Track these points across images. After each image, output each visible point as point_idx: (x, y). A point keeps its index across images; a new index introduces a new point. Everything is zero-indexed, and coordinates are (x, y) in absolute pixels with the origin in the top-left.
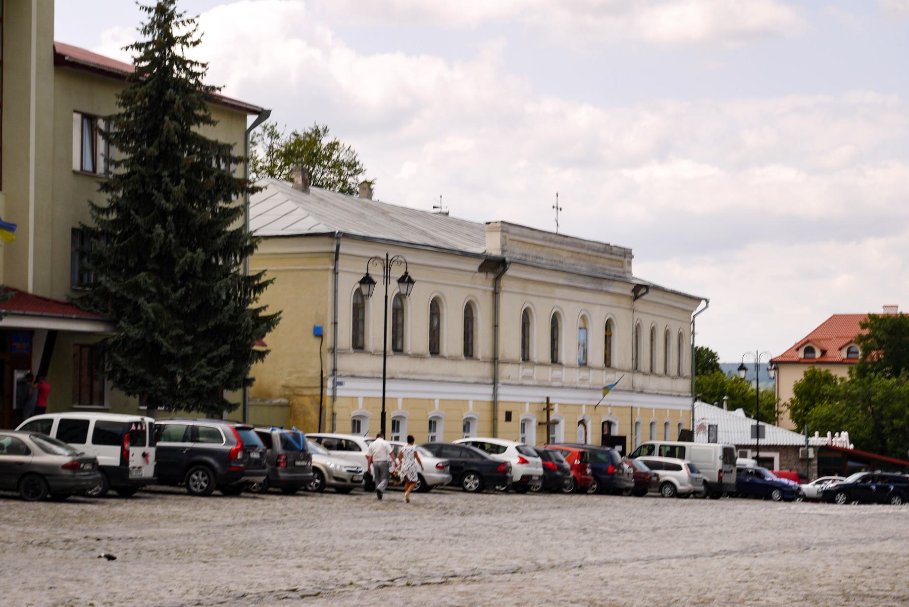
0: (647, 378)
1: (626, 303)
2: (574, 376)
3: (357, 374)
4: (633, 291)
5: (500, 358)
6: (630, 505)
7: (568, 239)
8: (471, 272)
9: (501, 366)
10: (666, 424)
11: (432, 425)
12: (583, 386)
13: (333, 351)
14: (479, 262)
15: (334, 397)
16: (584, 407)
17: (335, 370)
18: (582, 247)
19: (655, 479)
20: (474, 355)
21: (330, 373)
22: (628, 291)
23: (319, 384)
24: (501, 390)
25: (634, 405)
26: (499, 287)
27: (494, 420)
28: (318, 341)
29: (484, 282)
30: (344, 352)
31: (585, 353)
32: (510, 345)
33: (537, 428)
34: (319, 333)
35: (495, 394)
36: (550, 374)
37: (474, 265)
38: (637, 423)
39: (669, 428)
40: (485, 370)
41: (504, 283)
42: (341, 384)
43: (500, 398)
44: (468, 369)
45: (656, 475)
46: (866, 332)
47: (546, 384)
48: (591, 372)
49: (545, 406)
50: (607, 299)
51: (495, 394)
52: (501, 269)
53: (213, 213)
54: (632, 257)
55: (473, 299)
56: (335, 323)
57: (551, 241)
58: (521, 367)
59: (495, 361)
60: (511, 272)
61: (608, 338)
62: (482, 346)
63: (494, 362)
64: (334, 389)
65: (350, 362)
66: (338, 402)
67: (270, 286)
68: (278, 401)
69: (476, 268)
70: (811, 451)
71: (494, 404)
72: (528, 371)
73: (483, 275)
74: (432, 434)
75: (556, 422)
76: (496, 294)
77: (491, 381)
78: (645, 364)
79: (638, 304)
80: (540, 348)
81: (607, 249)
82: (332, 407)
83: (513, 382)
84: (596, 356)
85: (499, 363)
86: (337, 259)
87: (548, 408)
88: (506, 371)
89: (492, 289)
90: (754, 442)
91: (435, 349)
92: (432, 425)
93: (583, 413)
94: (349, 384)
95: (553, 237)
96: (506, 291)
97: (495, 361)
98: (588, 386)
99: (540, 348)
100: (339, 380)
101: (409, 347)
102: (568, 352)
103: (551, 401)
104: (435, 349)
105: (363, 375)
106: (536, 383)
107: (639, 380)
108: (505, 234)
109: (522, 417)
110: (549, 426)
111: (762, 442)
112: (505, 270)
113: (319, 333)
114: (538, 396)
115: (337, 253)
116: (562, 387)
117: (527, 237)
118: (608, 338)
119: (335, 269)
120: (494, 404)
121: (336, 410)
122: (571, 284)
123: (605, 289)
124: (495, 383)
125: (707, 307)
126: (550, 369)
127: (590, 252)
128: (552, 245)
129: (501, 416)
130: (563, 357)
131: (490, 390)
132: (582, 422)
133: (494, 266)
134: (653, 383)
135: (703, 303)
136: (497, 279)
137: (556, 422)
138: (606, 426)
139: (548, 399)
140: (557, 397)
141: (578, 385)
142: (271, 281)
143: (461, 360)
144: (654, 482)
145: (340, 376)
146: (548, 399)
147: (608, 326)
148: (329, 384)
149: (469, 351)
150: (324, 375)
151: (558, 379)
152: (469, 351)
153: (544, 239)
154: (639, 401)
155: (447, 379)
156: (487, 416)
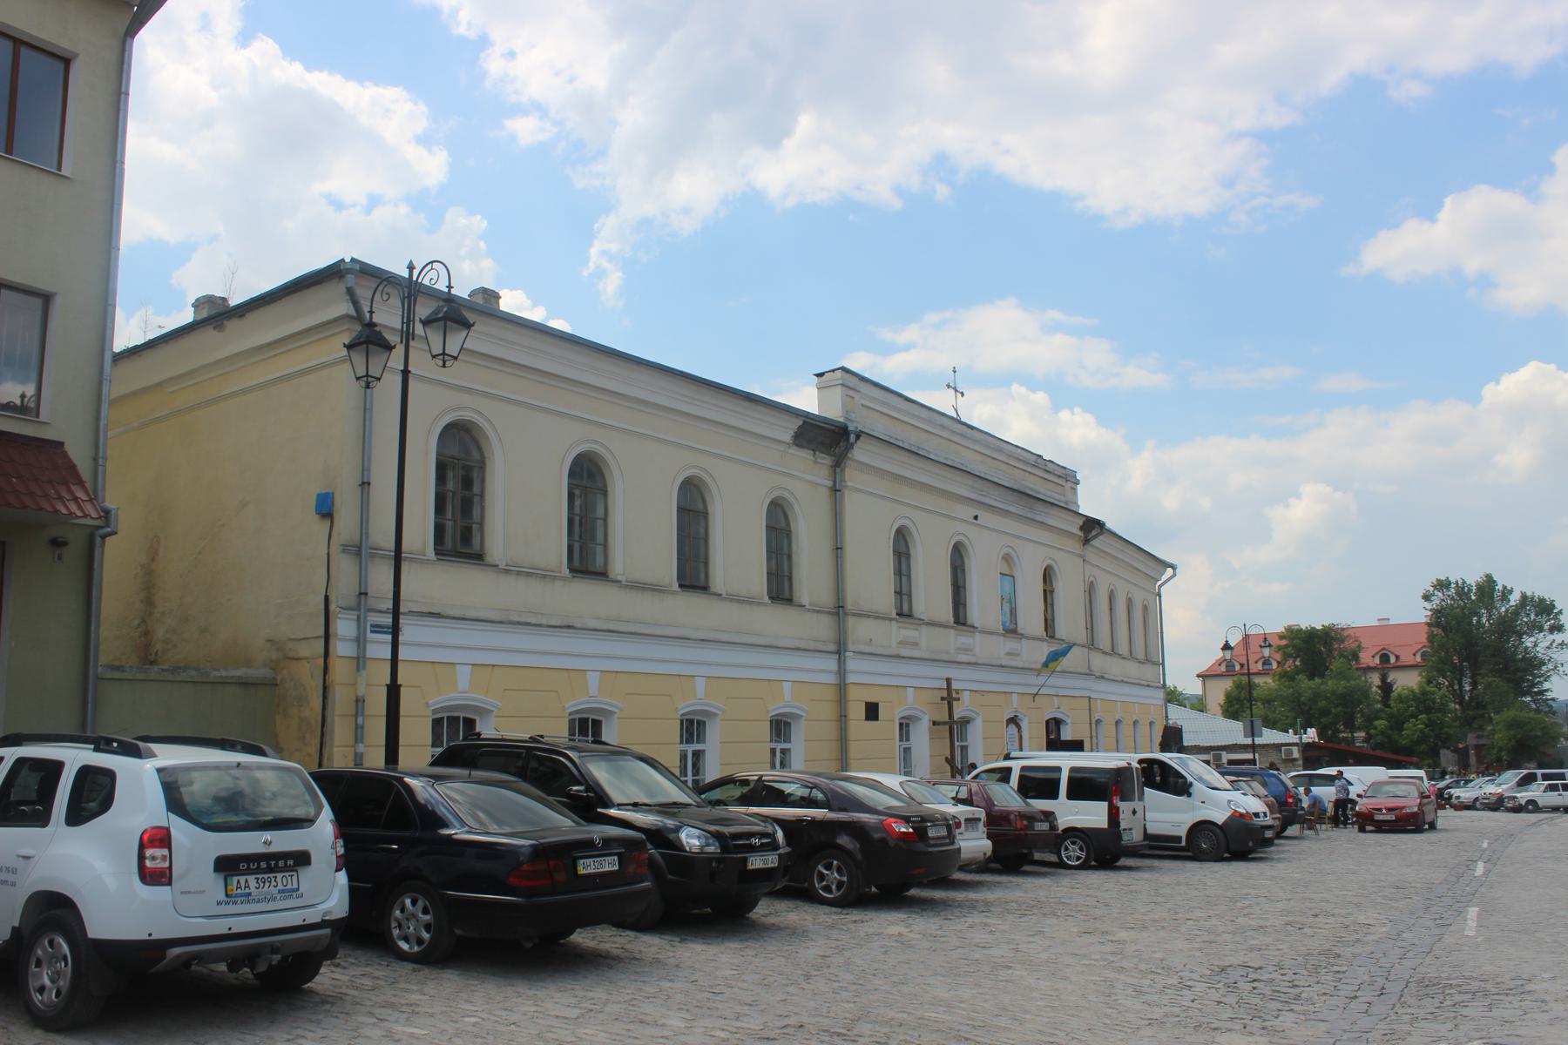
0: (1108, 658)
1: (1074, 546)
2: (999, 648)
4: (1082, 528)
5: (849, 606)
6: (865, 929)
7: (974, 433)
9: (851, 621)
10: (1135, 723)
11: (693, 728)
12: (1013, 663)
16: (787, 687)
18: (1000, 451)
19: (1042, 827)
22: (1074, 527)
23: (322, 632)
24: (852, 664)
26: (843, 480)
27: (842, 718)
31: (1013, 613)
32: (871, 581)
33: (931, 732)
34: (326, 509)
35: (841, 672)
36: (952, 640)
37: (786, 430)
38: (1098, 721)
39: (1122, 727)
40: (822, 627)
41: (852, 476)
43: (851, 678)
45: (1049, 816)
46: (1284, 642)
47: (946, 657)
48: (1024, 642)
49: (945, 694)
50: (1044, 536)
51: (841, 672)
54: (1077, 483)
55: (786, 495)
57: (942, 427)
60: (861, 453)
61: (1048, 594)
62: (811, 578)
69: (787, 436)
70: (1295, 749)
71: (842, 688)
72: (908, 632)
74: (905, 744)
75: (965, 722)
76: (835, 490)
77: (832, 647)
78: (1103, 641)
79: (1090, 553)
80: (932, 595)
81: (1038, 463)
83: (879, 651)
84: (1031, 619)
85: (846, 614)
87: (950, 698)
88: (860, 631)
89: (830, 483)
90: (1249, 741)
91: (693, 574)
92: (693, 728)
93: (1015, 705)
95: (947, 422)
96: (450, 287)
97: (839, 610)
98: (1020, 665)
99: (932, 595)
101: (621, 561)
102: (983, 605)
103: (955, 686)
104: (693, 574)
106: (926, 655)
107: (1098, 662)
108: (851, 393)
109: (898, 715)
110: (953, 728)
111: (1258, 741)
112: (850, 447)
113: (326, 509)
114: (933, 677)
117: (918, 418)
118: (1048, 594)
120: (842, 688)
122: (982, 499)
123: (1038, 518)
124: (840, 651)
126: (952, 632)
128: (946, 434)
129: (857, 711)
130: (974, 614)
132: (1013, 720)
133: (827, 439)
134: (1116, 667)
135: (1169, 571)
136: (838, 464)
137: (965, 722)
138: (1052, 725)
139: (948, 681)
140: (963, 680)
141: (1004, 662)
143: (759, 604)
144: (1041, 835)
146: (948, 681)
147: (1048, 575)
149: (781, 589)
150: (332, 607)
151: (967, 650)
152: (781, 589)
154: (1098, 689)
155: (725, 637)
156: (827, 711)
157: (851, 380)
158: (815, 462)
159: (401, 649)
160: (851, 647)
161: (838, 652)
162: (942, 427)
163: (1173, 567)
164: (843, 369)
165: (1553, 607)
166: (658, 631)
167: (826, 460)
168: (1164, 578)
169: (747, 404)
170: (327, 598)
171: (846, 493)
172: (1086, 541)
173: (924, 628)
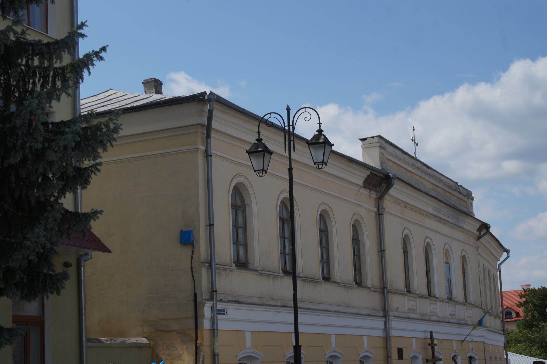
3: (242, 300)
7: (429, 171)
8: (357, 185)
9: (390, 296)
13: (210, 264)
14: (365, 173)
15: (214, 331)
17: (213, 292)
18: (440, 181)
20: (363, 284)
21: (207, 295)
22: (474, 228)
23: (191, 314)
24: (394, 324)
25: (487, 342)
28: (187, 251)
29: (366, 201)
30: (225, 267)
35: (387, 329)
37: (359, 177)
41: (387, 203)
42: (222, 312)
43: (393, 333)
44: (365, 299)
46: (524, 299)
47: (427, 318)
51: (387, 329)
52: (384, 186)
53: (27, 65)
56: (211, 226)
57: (418, 168)
58: (406, 298)
59: (384, 290)
60: (396, 191)
62: (371, 276)
63: (383, 293)
64: (213, 320)
65: (232, 282)
66: (220, 340)
67: (97, 67)
68: (133, 340)
69: (360, 181)
71: (387, 339)
73: (366, 192)
77: (381, 314)
79: (478, 243)
81: (456, 188)
82: (212, 346)
86: (208, 136)
88: (397, 302)
94: (233, 312)
100: (220, 306)
103: (435, 336)
105: (250, 300)
106: (420, 317)
108: (383, 151)
113: (187, 239)
115: (209, 127)
116: (439, 321)
119: (206, 151)
120: (387, 339)
121: (217, 350)
123: (461, 225)
125: (508, 257)
127: (445, 188)
129: (394, 354)
131: (380, 324)
133: (379, 181)
135: (505, 254)
136: (380, 199)
139: (431, 333)
142: (97, 55)
145: (221, 301)
146: (431, 333)
148: (207, 311)
150: (199, 300)
153: (413, 165)
155: (341, 309)
157: (383, 143)
158: (370, 197)
159: (292, 320)
160: (391, 314)
161: (385, 316)
162: (418, 168)
163: (508, 251)
164: (380, 137)
165: (87, 185)
166: (316, 307)
167: (374, 195)
168: (502, 259)
169: (349, 164)
170: (195, 294)
171: (384, 215)
172: (479, 238)
173: (418, 300)
